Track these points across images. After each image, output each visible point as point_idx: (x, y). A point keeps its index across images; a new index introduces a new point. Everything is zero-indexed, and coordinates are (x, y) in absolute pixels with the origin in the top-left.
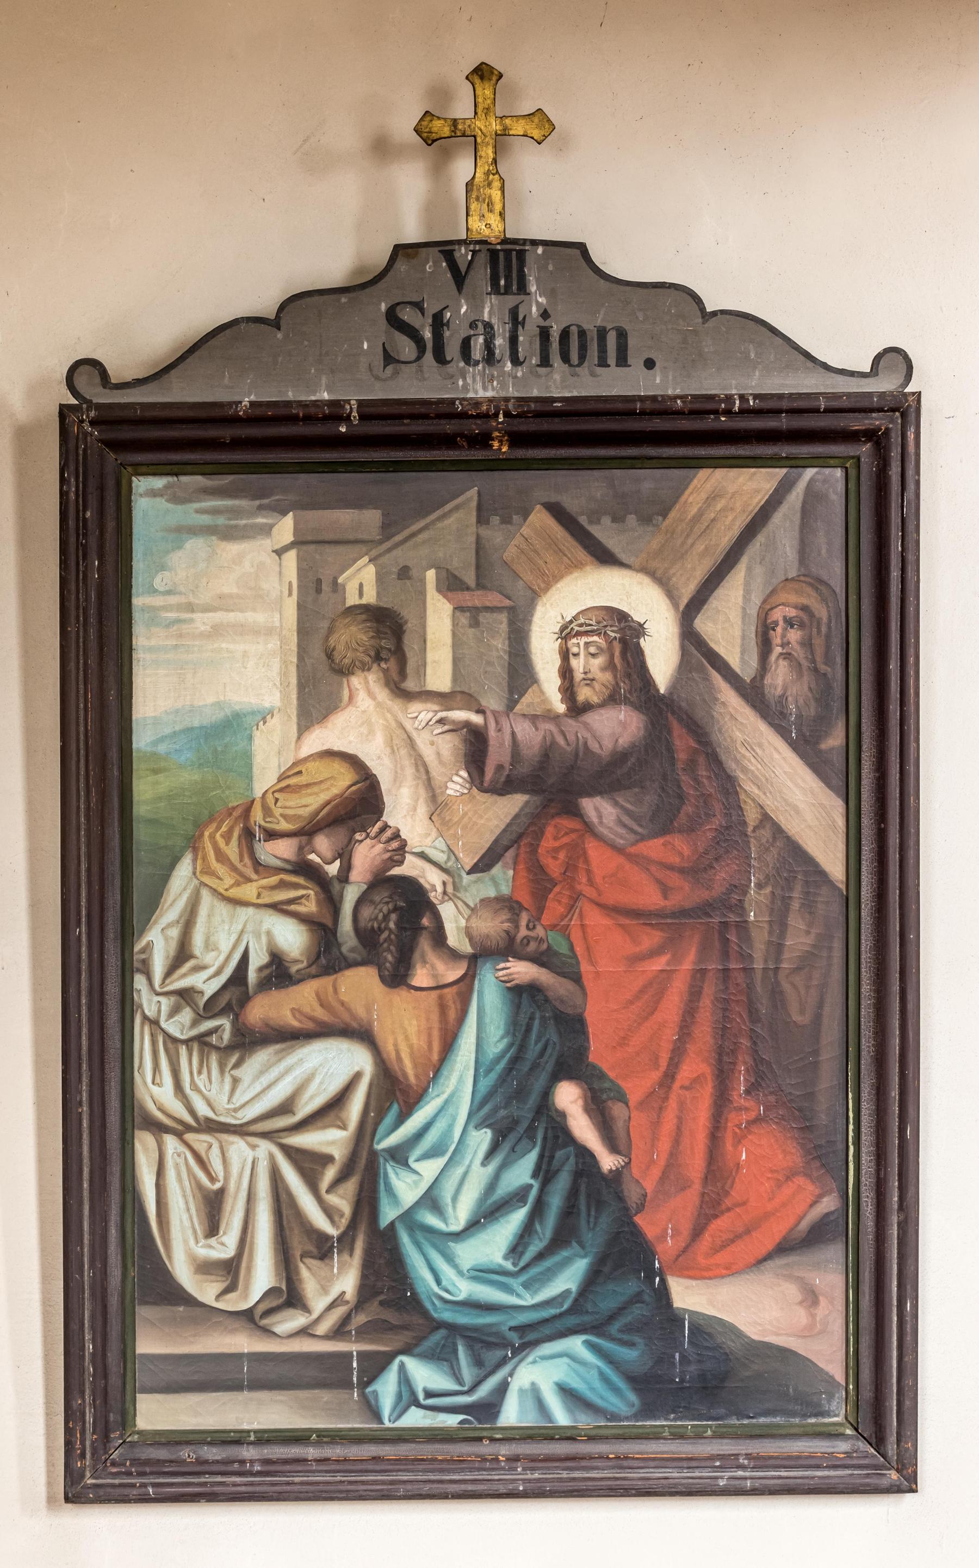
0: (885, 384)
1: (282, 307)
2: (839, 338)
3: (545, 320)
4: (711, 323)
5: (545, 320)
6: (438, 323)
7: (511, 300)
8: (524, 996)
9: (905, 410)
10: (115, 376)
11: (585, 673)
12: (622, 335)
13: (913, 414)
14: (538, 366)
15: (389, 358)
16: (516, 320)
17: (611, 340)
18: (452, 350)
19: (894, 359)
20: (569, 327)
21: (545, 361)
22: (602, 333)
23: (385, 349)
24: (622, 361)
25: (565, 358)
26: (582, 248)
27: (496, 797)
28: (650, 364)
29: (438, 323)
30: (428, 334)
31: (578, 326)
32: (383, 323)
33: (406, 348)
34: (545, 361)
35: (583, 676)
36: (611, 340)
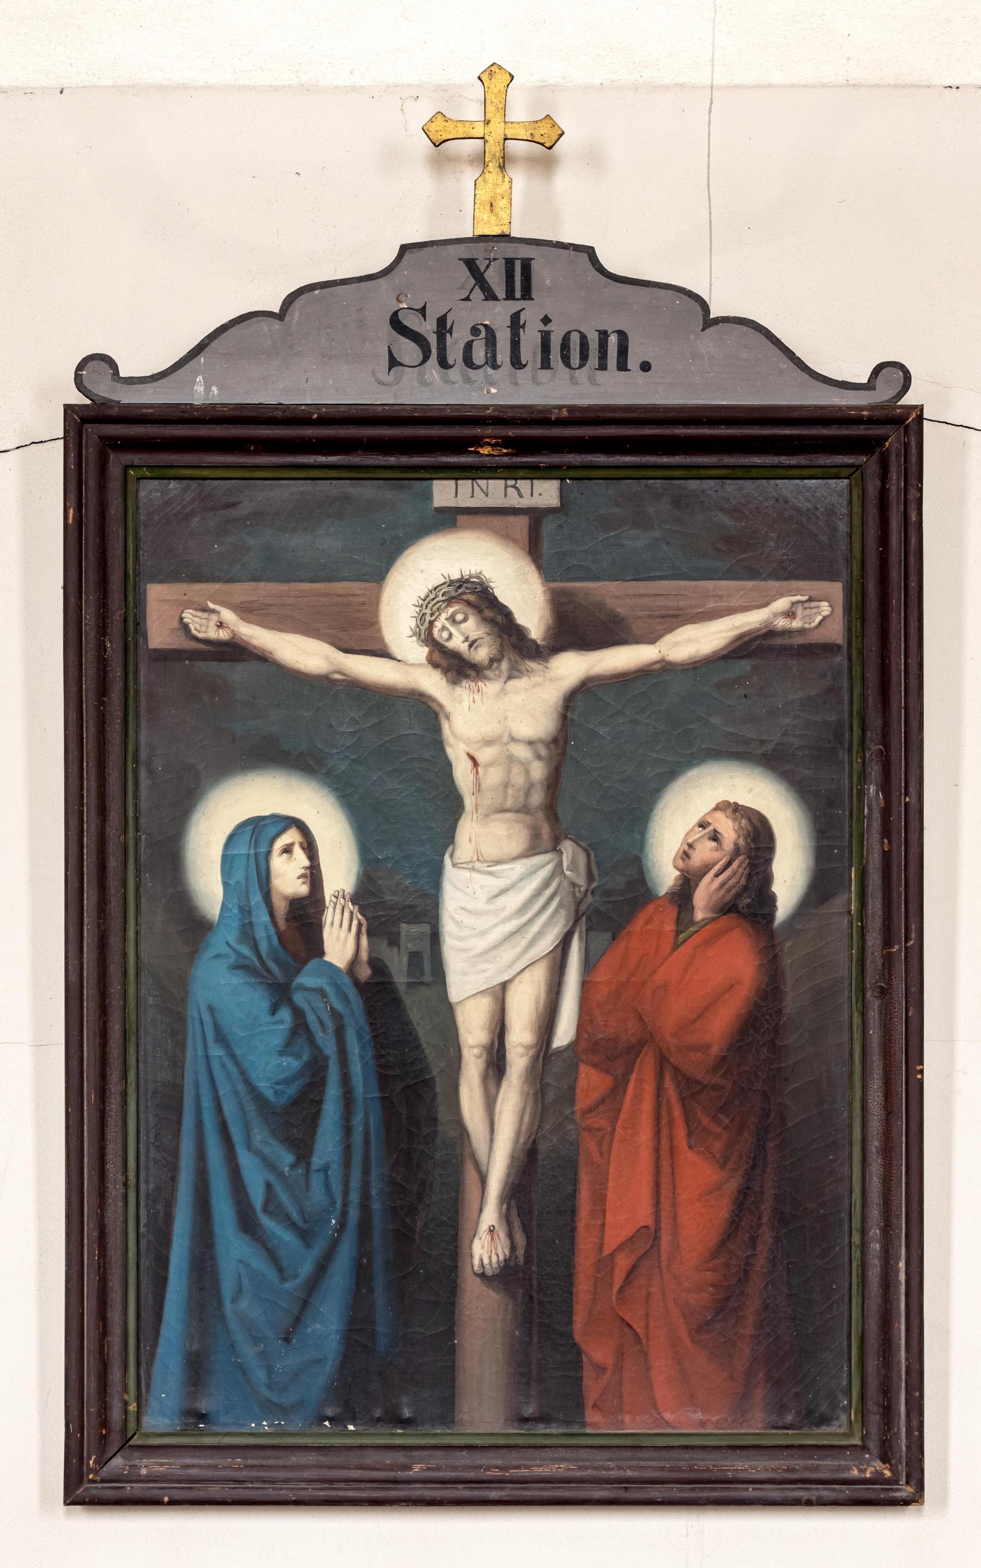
0: (882, 395)
1: (290, 299)
2: (840, 351)
3: (546, 325)
4: (708, 342)
5: (546, 325)
6: (443, 326)
7: (514, 306)
8: (448, 327)
9: (909, 424)
10: (123, 374)
11: (467, 639)
12: (622, 335)
13: (374, 1192)
14: (482, 1276)
15: (393, 362)
16: (516, 323)
17: (613, 339)
18: (455, 354)
19: (894, 373)
20: (569, 333)
21: (546, 364)
22: (603, 335)
23: (390, 352)
24: (622, 366)
25: (566, 360)
26: (590, 252)
27: (505, 1078)
28: (646, 367)
29: (443, 326)
30: (433, 340)
31: (485, 326)
32: (387, 327)
33: (408, 351)
34: (546, 364)
35: (467, 644)
36: (613, 339)
